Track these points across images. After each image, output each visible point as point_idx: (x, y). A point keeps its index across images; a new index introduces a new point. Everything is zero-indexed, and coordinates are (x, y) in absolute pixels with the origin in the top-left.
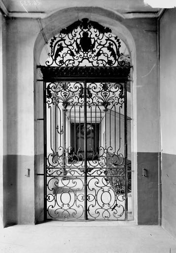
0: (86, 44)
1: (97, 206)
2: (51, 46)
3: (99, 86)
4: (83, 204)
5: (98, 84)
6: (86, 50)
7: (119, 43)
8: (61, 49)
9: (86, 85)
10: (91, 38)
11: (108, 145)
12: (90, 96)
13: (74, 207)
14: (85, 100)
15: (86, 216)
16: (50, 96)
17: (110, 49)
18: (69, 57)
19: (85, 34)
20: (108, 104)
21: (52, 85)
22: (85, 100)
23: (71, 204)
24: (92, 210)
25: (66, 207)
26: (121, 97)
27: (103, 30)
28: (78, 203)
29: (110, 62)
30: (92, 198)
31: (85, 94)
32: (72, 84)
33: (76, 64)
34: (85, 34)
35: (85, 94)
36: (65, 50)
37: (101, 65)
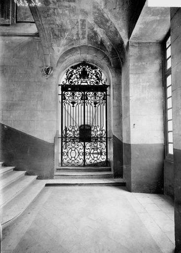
0: (84, 75)
1: (68, 159)
2: (67, 75)
3: (70, 94)
4: (83, 157)
5: (91, 93)
6: (84, 78)
7: (101, 74)
8: (72, 76)
9: (84, 93)
10: (87, 71)
11: (74, 125)
12: (87, 99)
13: (78, 159)
14: (84, 101)
15: (62, 164)
16: (65, 99)
17: (96, 76)
18: (76, 79)
19: (84, 69)
20: (75, 103)
21: (66, 93)
22: (84, 101)
23: (76, 157)
24: (65, 161)
25: (73, 159)
26: (103, 99)
27: (93, 68)
28: (80, 157)
29: (97, 83)
30: (81, 154)
31: (84, 98)
32: (99, 93)
33: (79, 84)
34: (84, 69)
35: (84, 98)
36: (74, 76)
37: (92, 84)
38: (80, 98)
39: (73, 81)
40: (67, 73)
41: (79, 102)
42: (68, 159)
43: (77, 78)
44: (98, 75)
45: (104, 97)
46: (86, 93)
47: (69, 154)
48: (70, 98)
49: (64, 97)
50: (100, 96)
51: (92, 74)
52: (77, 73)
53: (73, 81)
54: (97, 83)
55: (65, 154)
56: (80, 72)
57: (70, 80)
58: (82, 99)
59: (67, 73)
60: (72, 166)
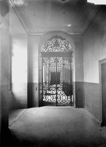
5: (61, 58)
6: (57, 46)
9: (57, 58)
12: (58, 62)
14: (57, 63)
17: (65, 45)
19: (57, 41)
21: (59, 58)
22: (57, 63)
30: (59, 98)
34: (57, 41)
36: (49, 46)
37: (62, 51)
38: (53, 61)
39: (49, 49)
40: (45, 43)
41: (53, 63)
42: (61, 101)
43: (52, 48)
44: (67, 45)
45: (55, 60)
46: (57, 58)
47: (61, 98)
48: (47, 62)
49: (58, 60)
50: (52, 60)
51: (61, 44)
52: (51, 44)
53: (49, 49)
54: (65, 50)
55: (54, 98)
56: (54, 43)
57: (47, 49)
58: (55, 62)
59: (45, 43)
60: (63, 106)
